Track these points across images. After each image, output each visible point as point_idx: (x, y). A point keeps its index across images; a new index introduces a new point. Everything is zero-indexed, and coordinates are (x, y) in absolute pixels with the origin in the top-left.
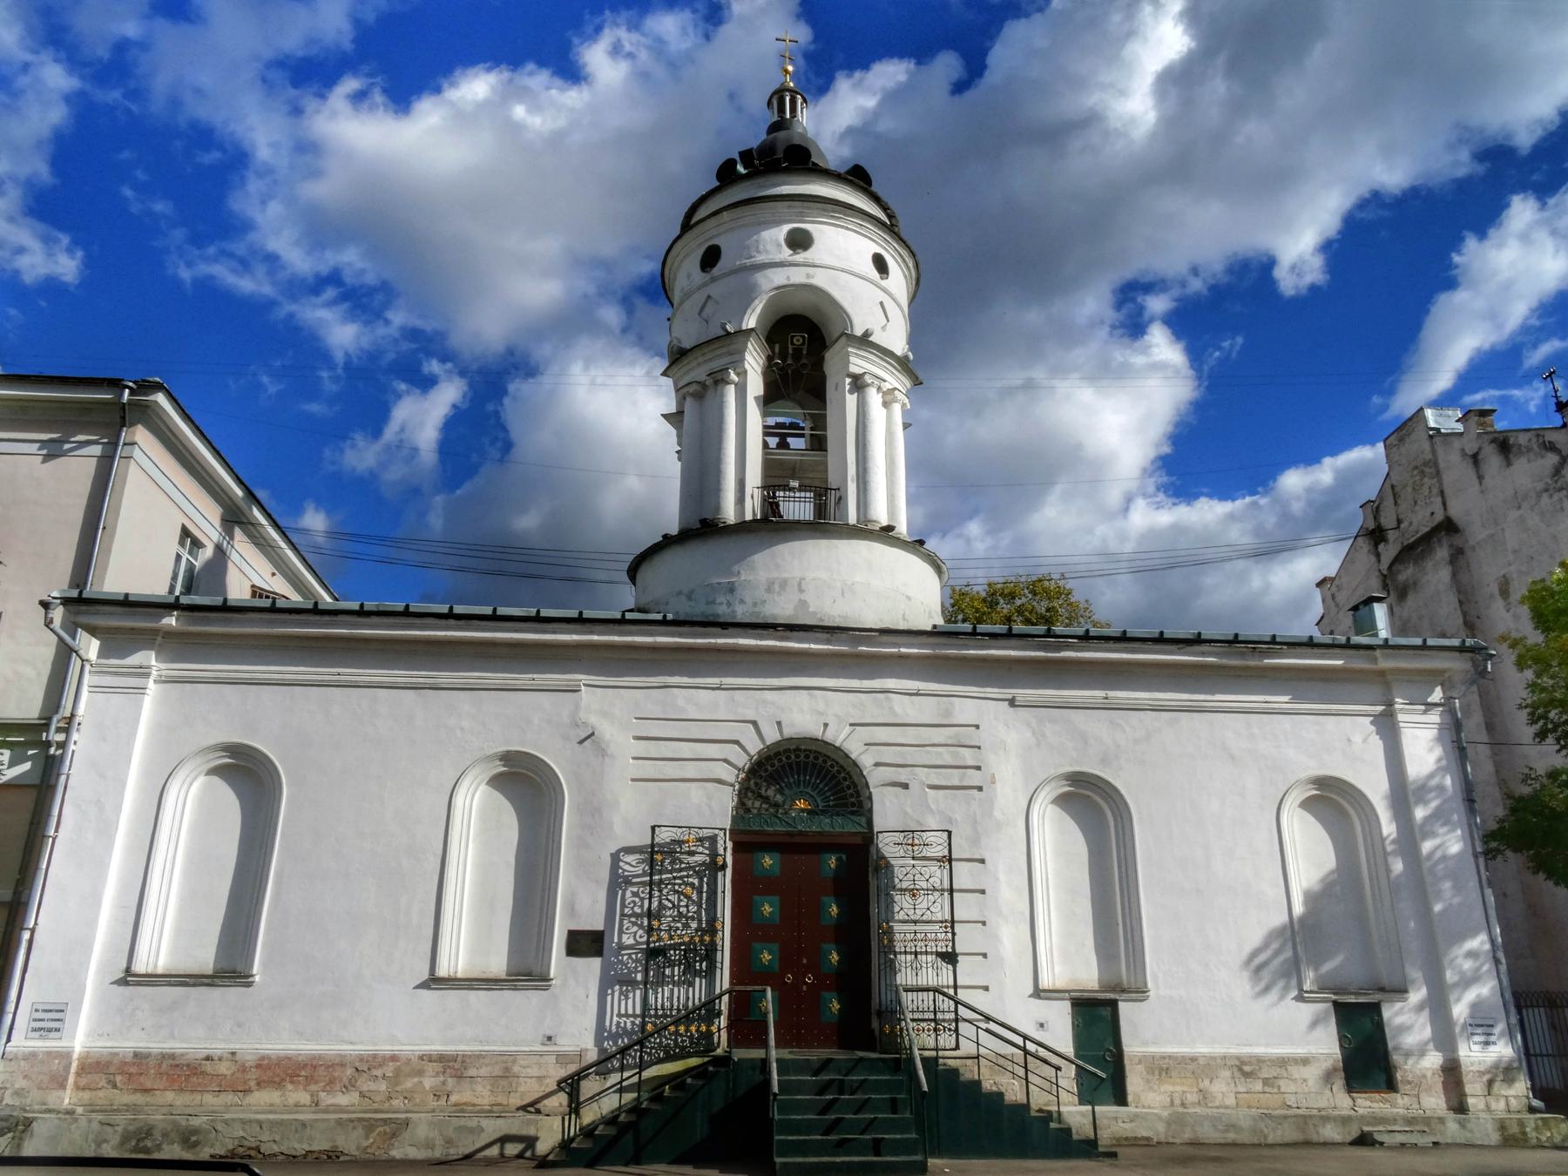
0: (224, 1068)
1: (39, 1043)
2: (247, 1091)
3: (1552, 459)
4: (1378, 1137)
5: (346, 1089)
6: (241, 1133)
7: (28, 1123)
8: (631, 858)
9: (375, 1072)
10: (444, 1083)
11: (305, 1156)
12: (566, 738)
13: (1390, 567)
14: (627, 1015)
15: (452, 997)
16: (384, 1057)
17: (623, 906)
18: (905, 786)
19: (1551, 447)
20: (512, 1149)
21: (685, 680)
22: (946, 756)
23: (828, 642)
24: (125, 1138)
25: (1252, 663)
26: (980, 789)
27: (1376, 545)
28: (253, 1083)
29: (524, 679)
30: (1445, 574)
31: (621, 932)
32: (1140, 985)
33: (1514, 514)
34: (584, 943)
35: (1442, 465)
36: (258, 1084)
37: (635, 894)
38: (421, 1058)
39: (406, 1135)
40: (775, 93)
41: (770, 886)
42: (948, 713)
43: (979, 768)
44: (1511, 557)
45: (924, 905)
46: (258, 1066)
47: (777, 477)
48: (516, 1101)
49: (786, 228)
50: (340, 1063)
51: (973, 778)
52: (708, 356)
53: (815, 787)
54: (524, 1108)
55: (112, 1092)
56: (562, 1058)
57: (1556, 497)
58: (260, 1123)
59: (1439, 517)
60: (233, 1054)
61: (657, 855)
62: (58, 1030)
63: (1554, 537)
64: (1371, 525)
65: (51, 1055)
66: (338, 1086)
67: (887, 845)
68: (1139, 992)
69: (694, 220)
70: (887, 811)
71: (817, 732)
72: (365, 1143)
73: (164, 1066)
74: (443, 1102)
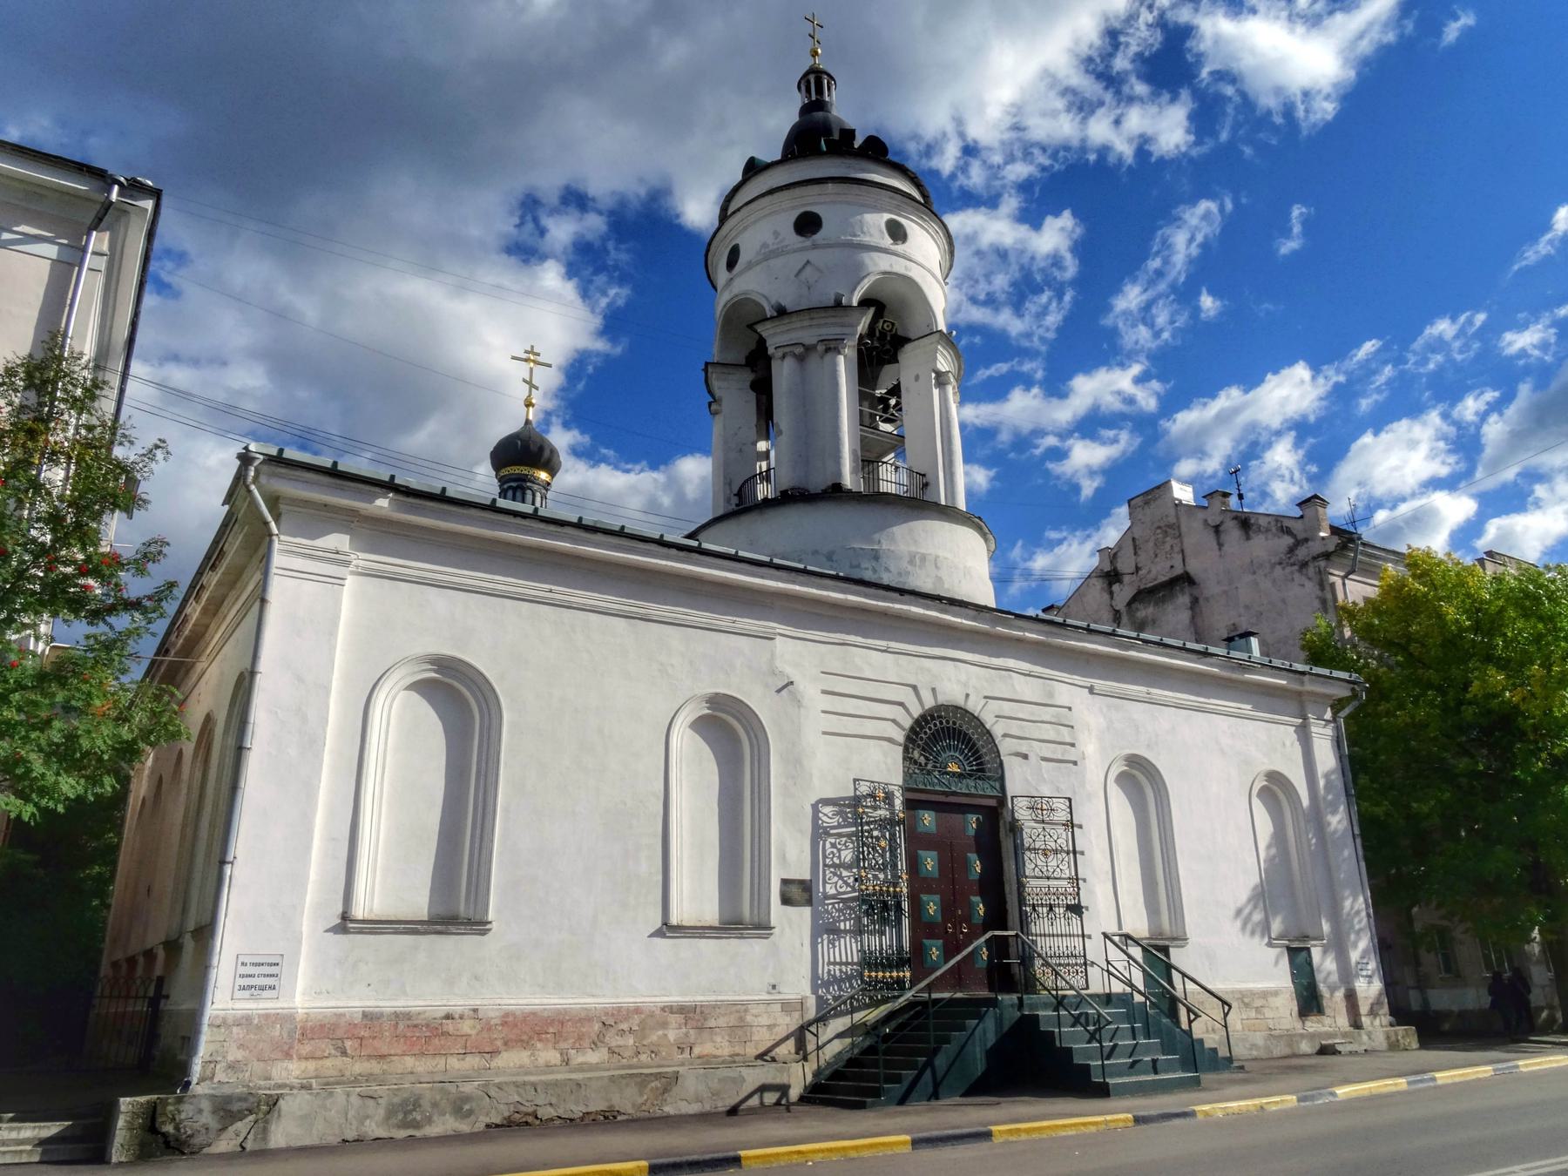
0: (467, 1027)
1: (251, 1005)
2: (494, 1053)
3: (1288, 540)
4: (1339, 1048)
5: (595, 1045)
6: (517, 1098)
7: (273, 1103)
8: (828, 810)
9: (625, 1026)
10: (686, 1035)
11: (582, 1119)
12: (767, 686)
13: (1129, 604)
14: (835, 963)
15: (685, 945)
16: (628, 1010)
17: (825, 857)
18: (1025, 757)
20: (770, 1098)
21: (859, 640)
23: (974, 619)
24: (391, 1112)
25: (1235, 676)
26: (1075, 763)
27: (1110, 585)
28: (499, 1043)
29: (725, 621)
30: (1185, 616)
31: (825, 882)
32: (1180, 934)
33: (1249, 578)
34: (798, 892)
35: (1184, 529)
36: (506, 1044)
37: (833, 845)
38: (663, 1009)
39: (676, 1090)
41: (928, 841)
42: (1051, 695)
43: (1073, 745)
44: (1242, 610)
45: (1054, 863)
46: (504, 1024)
48: (752, 1051)
49: (887, 216)
50: (585, 1018)
51: (1071, 754)
52: (815, 322)
53: (962, 752)
54: (761, 1057)
55: (339, 1062)
56: (786, 1006)
57: (1289, 569)
58: (535, 1087)
59: (1179, 570)
60: (475, 1011)
61: (852, 807)
62: (273, 988)
63: (1284, 601)
64: (1107, 568)
65: (269, 1019)
66: (586, 1043)
67: (1022, 813)
68: (1181, 939)
70: (1019, 780)
71: (960, 702)
72: (640, 1100)
73: (401, 1026)
74: (686, 1055)
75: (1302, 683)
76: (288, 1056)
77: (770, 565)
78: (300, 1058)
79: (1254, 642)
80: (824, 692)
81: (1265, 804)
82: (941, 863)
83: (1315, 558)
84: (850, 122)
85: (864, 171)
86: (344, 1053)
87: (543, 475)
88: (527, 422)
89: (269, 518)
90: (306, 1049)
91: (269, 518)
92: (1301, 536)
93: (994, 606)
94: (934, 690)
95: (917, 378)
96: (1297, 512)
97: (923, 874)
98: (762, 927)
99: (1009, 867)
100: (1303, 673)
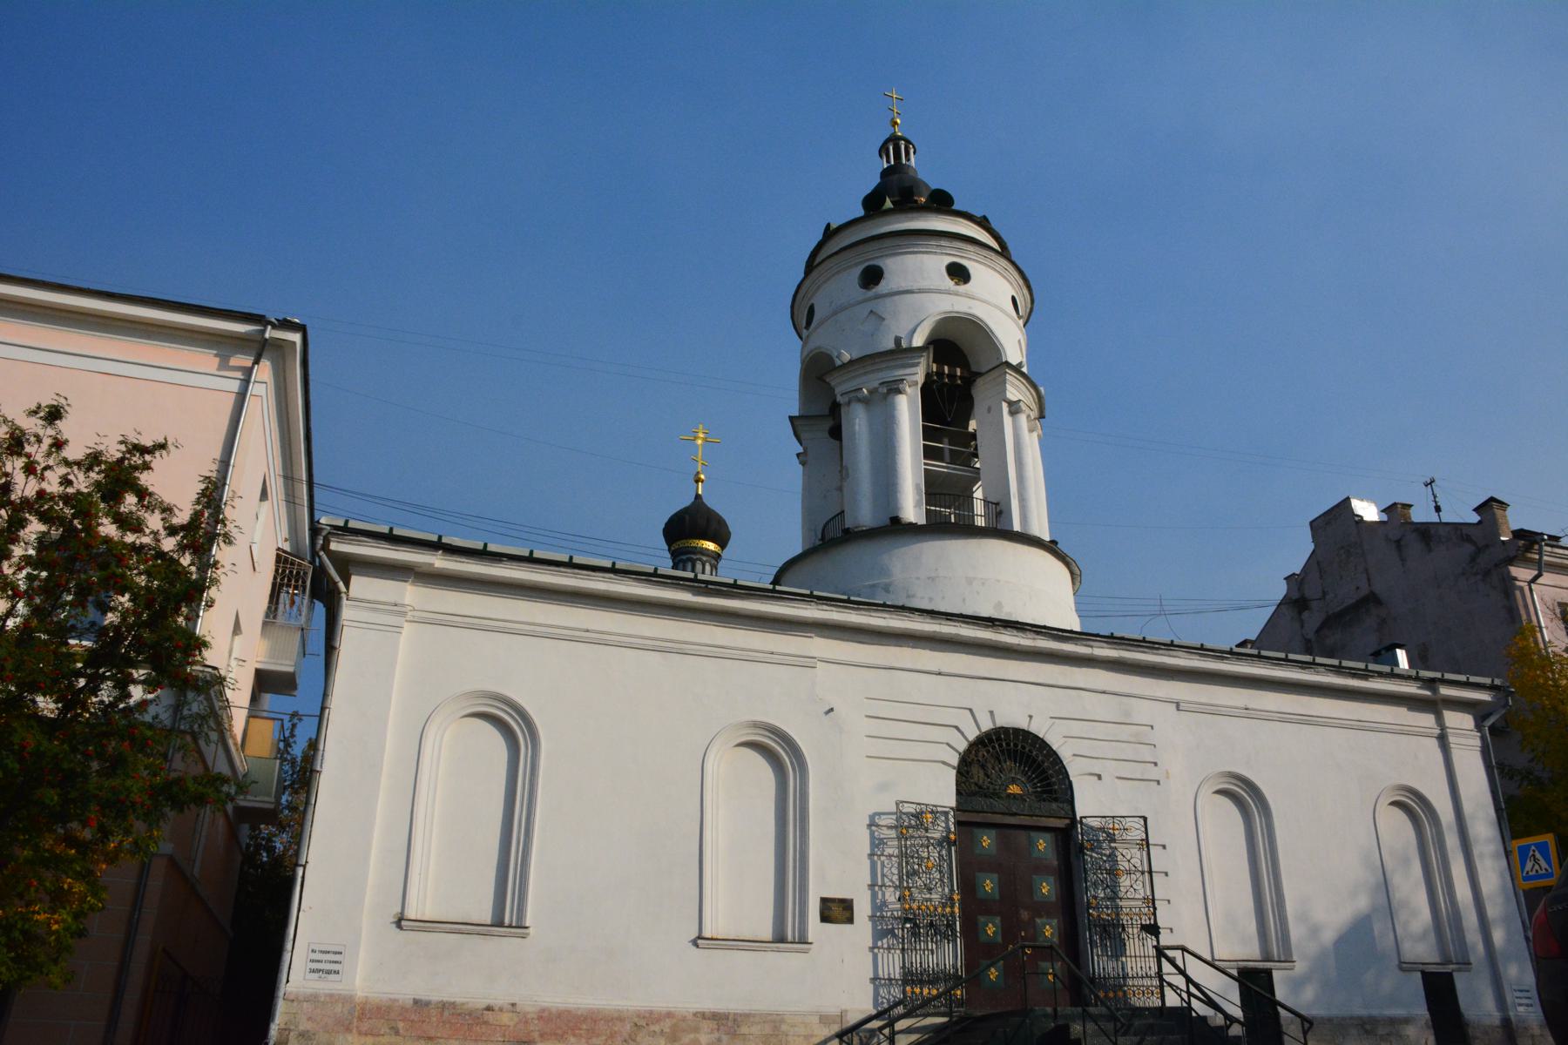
0: (506, 1018)
3: (1469, 549)
9: (656, 1028)
16: (660, 1014)
22: (1128, 751)
28: (536, 1035)
36: (542, 1036)
38: (695, 1014)
41: (990, 865)
46: (540, 1018)
47: (935, 489)
51: (1153, 773)
59: (1364, 591)
60: (513, 1005)
62: (337, 972)
64: (1295, 596)
65: (333, 999)
69: (818, 260)
70: (1089, 803)
71: (1021, 723)
73: (446, 1013)
76: (348, 1030)
77: (848, 601)
78: (360, 1033)
79: (1401, 655)
82: (1002, 886)
84: (922, 175)
85: (889, 224)
86: (397, 1033)
87: (711, 546)
88: (698, 497)
89: (337, 578)
90: (365, 1026)
91: (337, 578)
93: (1078, 629)
94: (991, 713)
95: (989, 410)
96: (1475, 518)
97: (980, 895)
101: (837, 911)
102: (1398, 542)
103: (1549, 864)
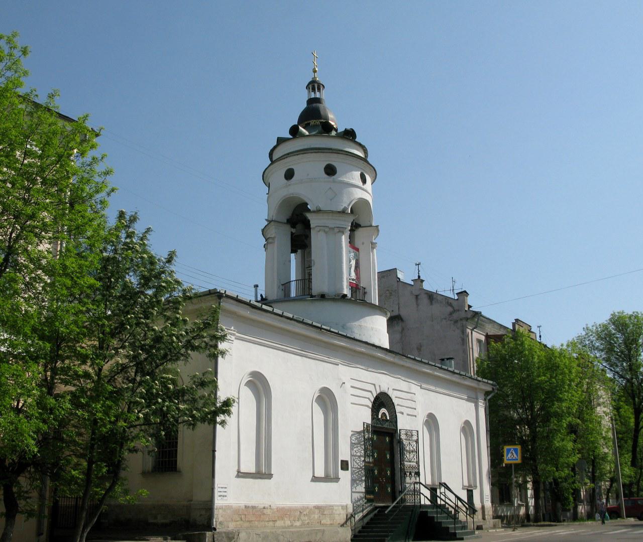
3: (450, 309)
9: (305, 513)
19: (450, 305)
26: (416, 416)
40: (310, 83)
43: (415, 409)
46: (277, 511)
50: (295, 510)
75: (478, 385)
80: (352, 387)
81: (319, 405)
83: (461, 320)
92: (456, 308)
94: (380, 386)
95: (363, 243)
96: (456, 297)
98: (336, 479)
99: (397, 456)
100: (480, 381)
101: (345, 465)
102: (417, 296)
103: (517, 456)
